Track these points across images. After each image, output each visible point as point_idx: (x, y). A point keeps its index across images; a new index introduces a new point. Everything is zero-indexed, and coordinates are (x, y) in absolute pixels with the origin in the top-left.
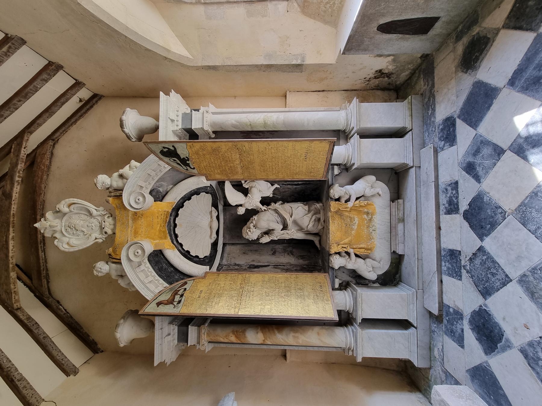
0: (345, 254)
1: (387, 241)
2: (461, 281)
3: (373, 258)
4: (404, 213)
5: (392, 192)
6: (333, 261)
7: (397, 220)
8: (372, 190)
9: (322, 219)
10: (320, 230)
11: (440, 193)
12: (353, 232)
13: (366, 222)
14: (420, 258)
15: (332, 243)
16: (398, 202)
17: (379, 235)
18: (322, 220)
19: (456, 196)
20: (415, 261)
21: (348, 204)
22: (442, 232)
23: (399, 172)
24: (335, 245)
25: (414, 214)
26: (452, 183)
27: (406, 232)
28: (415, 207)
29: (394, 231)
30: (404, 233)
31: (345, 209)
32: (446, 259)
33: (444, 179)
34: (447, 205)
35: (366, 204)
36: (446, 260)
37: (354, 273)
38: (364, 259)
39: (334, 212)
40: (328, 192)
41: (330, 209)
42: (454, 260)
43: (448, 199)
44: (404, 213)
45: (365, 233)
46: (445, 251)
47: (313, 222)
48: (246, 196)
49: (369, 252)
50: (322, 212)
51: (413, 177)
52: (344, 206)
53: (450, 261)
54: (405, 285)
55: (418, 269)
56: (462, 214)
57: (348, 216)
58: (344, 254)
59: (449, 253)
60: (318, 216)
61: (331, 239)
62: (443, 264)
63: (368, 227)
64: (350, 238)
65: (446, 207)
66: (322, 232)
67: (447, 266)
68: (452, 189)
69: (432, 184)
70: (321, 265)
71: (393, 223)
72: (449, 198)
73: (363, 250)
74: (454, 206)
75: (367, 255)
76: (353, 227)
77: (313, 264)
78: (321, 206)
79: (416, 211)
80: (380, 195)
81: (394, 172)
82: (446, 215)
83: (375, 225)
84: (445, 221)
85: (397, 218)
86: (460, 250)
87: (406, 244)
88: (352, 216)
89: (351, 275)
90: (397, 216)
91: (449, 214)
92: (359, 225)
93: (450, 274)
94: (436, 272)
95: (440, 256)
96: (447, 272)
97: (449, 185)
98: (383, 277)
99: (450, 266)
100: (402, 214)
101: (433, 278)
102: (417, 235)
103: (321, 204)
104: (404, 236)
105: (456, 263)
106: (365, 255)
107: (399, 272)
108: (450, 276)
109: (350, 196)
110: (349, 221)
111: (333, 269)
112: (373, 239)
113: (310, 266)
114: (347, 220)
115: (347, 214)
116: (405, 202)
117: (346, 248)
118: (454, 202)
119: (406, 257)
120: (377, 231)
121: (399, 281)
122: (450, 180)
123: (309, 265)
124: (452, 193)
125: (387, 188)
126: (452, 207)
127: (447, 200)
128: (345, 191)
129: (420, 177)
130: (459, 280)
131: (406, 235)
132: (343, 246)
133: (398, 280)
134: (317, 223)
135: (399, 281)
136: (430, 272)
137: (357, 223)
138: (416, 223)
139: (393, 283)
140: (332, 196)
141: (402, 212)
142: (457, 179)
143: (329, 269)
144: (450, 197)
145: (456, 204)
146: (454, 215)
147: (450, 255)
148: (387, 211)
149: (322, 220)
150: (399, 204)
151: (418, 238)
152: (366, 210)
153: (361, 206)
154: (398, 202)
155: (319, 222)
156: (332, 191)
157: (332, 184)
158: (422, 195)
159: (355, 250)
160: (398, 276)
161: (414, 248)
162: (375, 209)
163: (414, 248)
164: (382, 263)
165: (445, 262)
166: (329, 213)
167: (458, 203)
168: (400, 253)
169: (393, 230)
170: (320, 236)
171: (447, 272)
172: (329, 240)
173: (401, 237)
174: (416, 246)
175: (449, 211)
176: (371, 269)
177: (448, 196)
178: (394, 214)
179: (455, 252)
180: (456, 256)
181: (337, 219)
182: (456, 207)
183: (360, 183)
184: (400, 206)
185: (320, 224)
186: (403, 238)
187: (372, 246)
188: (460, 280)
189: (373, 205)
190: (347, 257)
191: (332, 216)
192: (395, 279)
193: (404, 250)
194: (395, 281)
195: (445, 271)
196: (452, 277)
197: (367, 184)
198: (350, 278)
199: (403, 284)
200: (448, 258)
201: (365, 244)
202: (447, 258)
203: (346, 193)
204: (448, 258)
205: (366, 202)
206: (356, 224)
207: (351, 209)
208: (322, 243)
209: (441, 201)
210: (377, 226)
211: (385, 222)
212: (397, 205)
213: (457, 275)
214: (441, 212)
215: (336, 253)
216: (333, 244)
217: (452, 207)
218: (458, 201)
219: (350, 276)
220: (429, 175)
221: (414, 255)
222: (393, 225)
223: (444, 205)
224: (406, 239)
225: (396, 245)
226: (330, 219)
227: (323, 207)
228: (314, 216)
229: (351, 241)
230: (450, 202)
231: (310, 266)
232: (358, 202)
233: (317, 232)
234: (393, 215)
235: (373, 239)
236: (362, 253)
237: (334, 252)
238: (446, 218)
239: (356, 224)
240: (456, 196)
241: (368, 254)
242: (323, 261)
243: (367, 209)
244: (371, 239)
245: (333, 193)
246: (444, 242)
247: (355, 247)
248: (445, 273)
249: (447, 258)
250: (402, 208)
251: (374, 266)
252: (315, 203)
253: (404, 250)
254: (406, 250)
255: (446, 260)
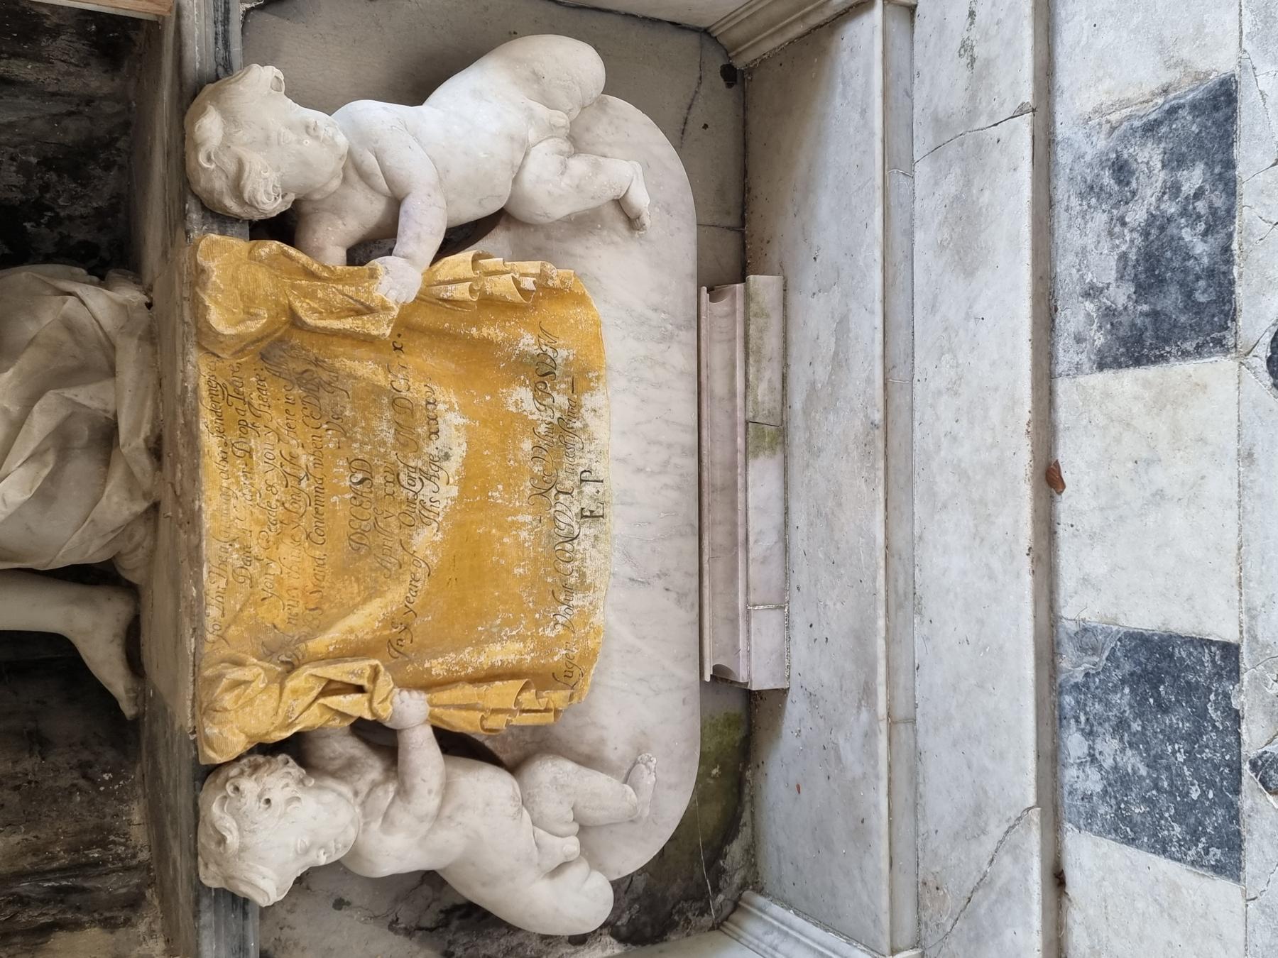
0: (352, 748)
1: (681, 597)
2: (1238, 879)
3: (585, 749)
4: (784, 378)
5: (708, 221)
6: (233, 839)
7: (740, 430)
8: (579, 166)
9: (135, 430)
10: (125, 530)
11: (1060, 209)
12: (425, 540)
13: (527, 445)
14: (900, 712)
15: (226, 651)
16: (748, 297)
17: (628, 556)
18: (132, 439)
19: (1213, 210)
20: (869, 735)
21: (373, 275)
22: (1066, 504)
23: (750, 70)
24: (255, 672)
25: (869, 381)
26: (1173, 111)
27: (799, 518)
28: (878, 321)
29: (719, 516)
30: (786, 524)
31: (348, 324)
32: (1098, 707)
33: (1107, 83)
34: (1121, 295)
35: (528, 283)
36: (1102, 720)
37: (427, 890)
38: (514, 768)
39: (243, 346)
40: (182, 143)
41: (198, 308)
42: (1172, 719)
43: (1130, 242)
44: (784, 378)
45: (520, 545)
46: (1095, 650)
47: (35, 456)
48: (1239, 880)
49: (557, 697)
50: (129, 359)
51: (868, 84)
52: (337, 293)
53: (1136, 726)
54: (789, 915)
55: (889, 794)
56: (1264, 351)
57: (377, 391)
58: (348, 747)
59: (1128, 667)
60: (88, 396)
61: (213, 612)
62: (1075, 744)
63: (546, 488)
64: (395, 596)
65: (1109, 313)
66: (141, 553)
67: (1108, 763)
68: (1175, 161)
69: (1016, 127)
70: (144, 856)
71: (717, 453)
72: (1146, 234)
73: (503, 693)
74: (1189, 295)
75: (535, 729)
76: (427, 492)
77: (64, 859)
78: (123, 307)
79: (884, 356)
80: (633, 222)
81: (721, 62)
82: (1109, 374)
83: (600, 470)
84: (1101, 420)
85: (740, 415)
86: (1231, 635)
87: (796, 607)
88: (416, 391)
89: (406, 916)
90: (739, 401)
91: (1138, 362)
92: (473, 478)
93: (1129, 821)
94: (1035, 816)
95: (1052, 690)
96: (1102, 810)
97: (1150, 129)
98: (640, 884)
99: (1133, 762)
100: (771, 390)
101: (1006, 860)
102: (887, 538)
103: (130, 295)
104: (786, 550)
105: (1193, 738)
106: (522, 728)
107: (746, 816)
108: (1130, 842)
109: (396, 203)
110: (389, 436)
111: (238, 903)
112: (583, 586)
113: (24, 887)
114: (369, 430)
115: (366, 368)
116: (795, 299)
117: (360, 689)
118: (1188, 256)
119: (795, 711)
120: (617, 523)
121: (744, 886)
122: (1155, 85)
123: (20, 876)
124: (1173, 189)
125: (677, 167)
126: (1170, 300)
127: (1123, 257)
128: (342, 140)
129: (909, 94)
130: (1218, 869)
131: (798, 540)
132: (337, 672)
133: (737, 879)
134: (81, 466)
135: (744, 886)
136: (978, 811)
137: (458, 453)
138: (880, 445)
139: (704, 911)
140: (220, 184)
141: (769, 375)
142: (1221, 63)
143: (196, 915)
144: (1157, 224)
145: (1211, 273)
146: (1190, 367)
147: (1132, 680)
148: (680, 358)
149: (132, 439)
150: (753, 307)
151: (894, 562)
152: (528, 342)
153: (489, 302)
154: (748, 297)
155: (107, 463)
156: (210, 127)
157: (225, 69)
158: (919, 236)
159: (445, 696)
160: (735, 850)
161: (861, 638)
162: (598, 338)
163: (861, 638)
164: (648, 780)
165: (1090, 734)
166: (194, 355)
167: (1229, 262)
168: (761, 680)
169: (716, 512)
170: (132, 591)
171: (1102, 810)
172: (198, 632)
173: (765, 561)
174: (881, 623)
175: (1139, 340)
176: (571, 845)
177: (1137, 215)
178: (718, 385)
179: (1181, 653)
180: (1191, 688)
181: (278, 420)
182: (1202, 298)
183: (477, 94)
184: (761, 321)
185: (117, 475)
186: (774, 571)
187: (576, 651)
188: (1230, 868)
189: (581, 300)
190: (374, 768)
191: (227, 394)
192: (717, 874)
193: (784, 657)
194: (716, 890)
195: (1087, 797)
196: (1152, 849)
197: (540, 110)
198: (400, 939)
199: (776, 909)
200: (1123, 698)
201: (522, 638)
202: (1108, 705)
203: (354, 169)
204: (1116, 698)
205: (533, 267)
206: (453, 466)
207: (407, 327)
208: (152, 652)
209: (1065, 267)
210: (615, 477)
211: (669, 446)
212: (739, 317)
213: (1194, 834)
214: (1066, 356)
215: (266, 750)
216: (239, 663)
217: (1170, 300)
218: (1226, 249)
219: (393, 926)
220: (988, 63)
221: (867, 692)
222: (715, 475)
223: (1092, 292)
224: (801, 576)
225: (733, 621)
226: (206, 421)
227: (143, 315)
228: (50, 398)
229: (402, 622)
230: (1150, 270)
231: (24, 887)
232: (460, 262)
233: (93, 553)
234: (712, 397)
235: (583, 586)
236: (497, 722)
237: (238, 744)
238: (1107, 395)
239: (453, 466)
240: (1213, 210)
241: (549, 718)
242: (157, 818)
243: (542, 332)
244: (569, 590)
245: (226, 145)
246: (1085, 580)
247: (437, 667)
248: (1091, 815)
249: (1108, 705)
250: (772, 343)
251: (596, 814)
252: (73, 278)
253: (784, 657)
254: (800, 652)
255: (1102, 720)
